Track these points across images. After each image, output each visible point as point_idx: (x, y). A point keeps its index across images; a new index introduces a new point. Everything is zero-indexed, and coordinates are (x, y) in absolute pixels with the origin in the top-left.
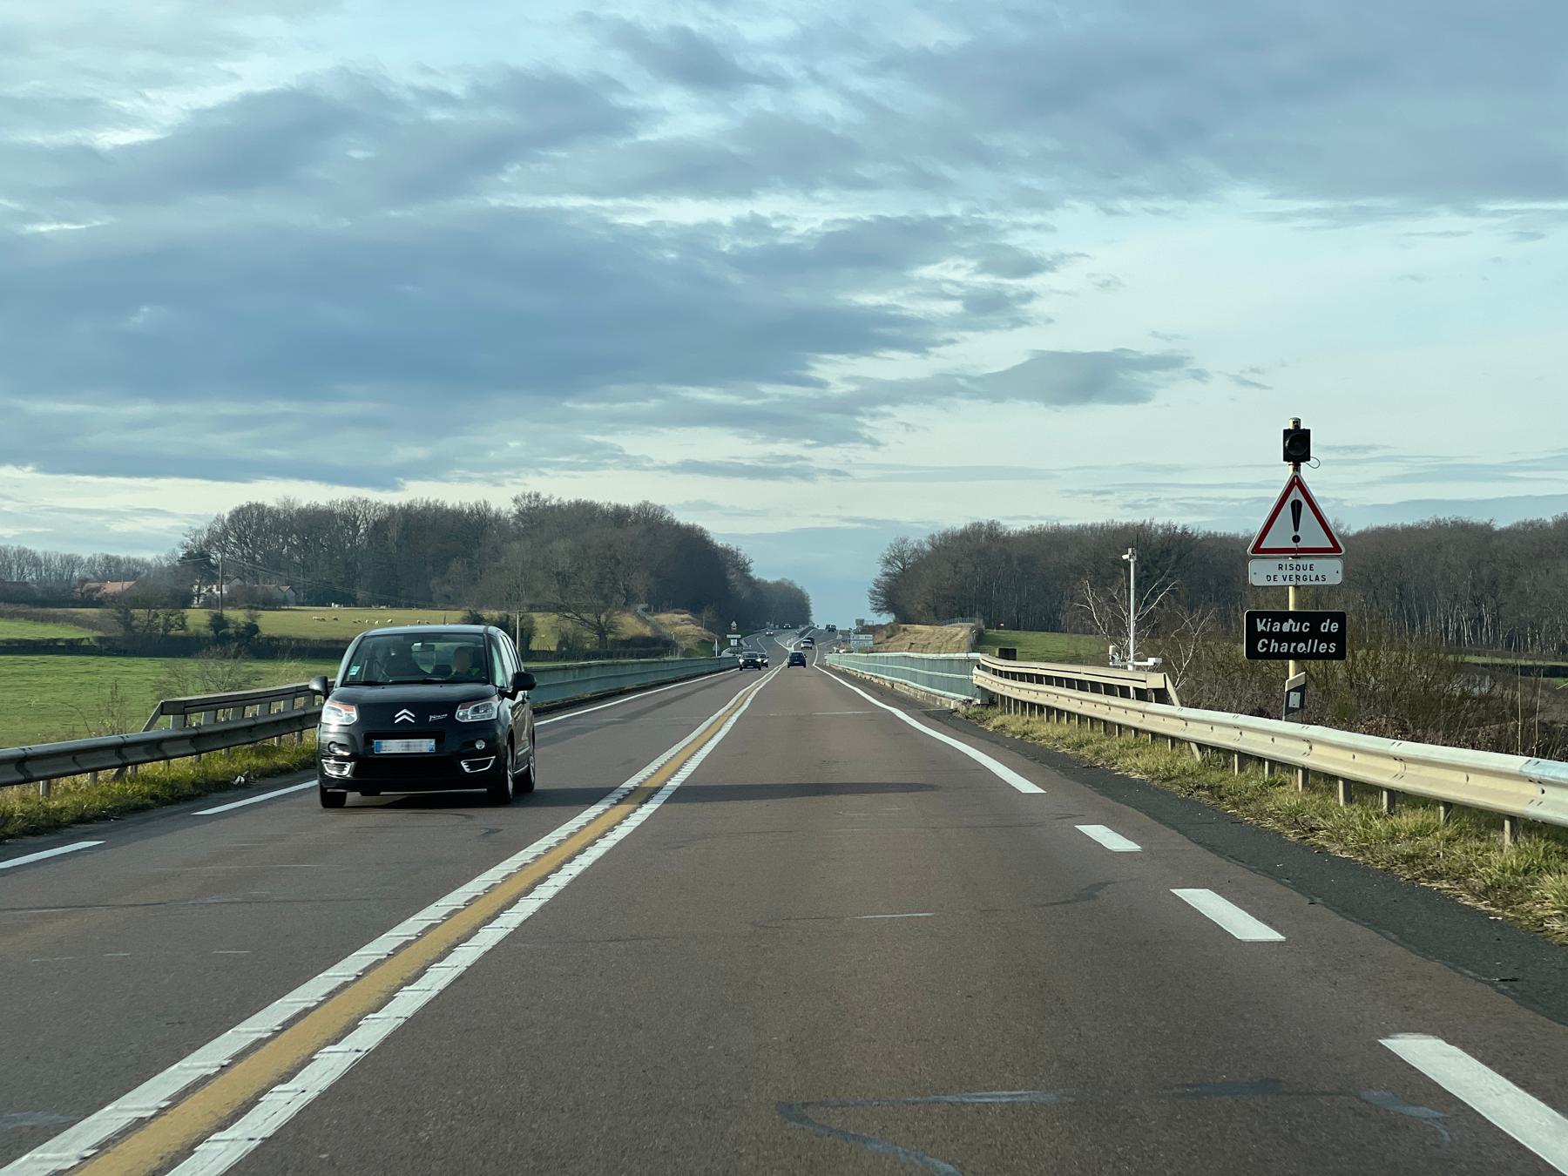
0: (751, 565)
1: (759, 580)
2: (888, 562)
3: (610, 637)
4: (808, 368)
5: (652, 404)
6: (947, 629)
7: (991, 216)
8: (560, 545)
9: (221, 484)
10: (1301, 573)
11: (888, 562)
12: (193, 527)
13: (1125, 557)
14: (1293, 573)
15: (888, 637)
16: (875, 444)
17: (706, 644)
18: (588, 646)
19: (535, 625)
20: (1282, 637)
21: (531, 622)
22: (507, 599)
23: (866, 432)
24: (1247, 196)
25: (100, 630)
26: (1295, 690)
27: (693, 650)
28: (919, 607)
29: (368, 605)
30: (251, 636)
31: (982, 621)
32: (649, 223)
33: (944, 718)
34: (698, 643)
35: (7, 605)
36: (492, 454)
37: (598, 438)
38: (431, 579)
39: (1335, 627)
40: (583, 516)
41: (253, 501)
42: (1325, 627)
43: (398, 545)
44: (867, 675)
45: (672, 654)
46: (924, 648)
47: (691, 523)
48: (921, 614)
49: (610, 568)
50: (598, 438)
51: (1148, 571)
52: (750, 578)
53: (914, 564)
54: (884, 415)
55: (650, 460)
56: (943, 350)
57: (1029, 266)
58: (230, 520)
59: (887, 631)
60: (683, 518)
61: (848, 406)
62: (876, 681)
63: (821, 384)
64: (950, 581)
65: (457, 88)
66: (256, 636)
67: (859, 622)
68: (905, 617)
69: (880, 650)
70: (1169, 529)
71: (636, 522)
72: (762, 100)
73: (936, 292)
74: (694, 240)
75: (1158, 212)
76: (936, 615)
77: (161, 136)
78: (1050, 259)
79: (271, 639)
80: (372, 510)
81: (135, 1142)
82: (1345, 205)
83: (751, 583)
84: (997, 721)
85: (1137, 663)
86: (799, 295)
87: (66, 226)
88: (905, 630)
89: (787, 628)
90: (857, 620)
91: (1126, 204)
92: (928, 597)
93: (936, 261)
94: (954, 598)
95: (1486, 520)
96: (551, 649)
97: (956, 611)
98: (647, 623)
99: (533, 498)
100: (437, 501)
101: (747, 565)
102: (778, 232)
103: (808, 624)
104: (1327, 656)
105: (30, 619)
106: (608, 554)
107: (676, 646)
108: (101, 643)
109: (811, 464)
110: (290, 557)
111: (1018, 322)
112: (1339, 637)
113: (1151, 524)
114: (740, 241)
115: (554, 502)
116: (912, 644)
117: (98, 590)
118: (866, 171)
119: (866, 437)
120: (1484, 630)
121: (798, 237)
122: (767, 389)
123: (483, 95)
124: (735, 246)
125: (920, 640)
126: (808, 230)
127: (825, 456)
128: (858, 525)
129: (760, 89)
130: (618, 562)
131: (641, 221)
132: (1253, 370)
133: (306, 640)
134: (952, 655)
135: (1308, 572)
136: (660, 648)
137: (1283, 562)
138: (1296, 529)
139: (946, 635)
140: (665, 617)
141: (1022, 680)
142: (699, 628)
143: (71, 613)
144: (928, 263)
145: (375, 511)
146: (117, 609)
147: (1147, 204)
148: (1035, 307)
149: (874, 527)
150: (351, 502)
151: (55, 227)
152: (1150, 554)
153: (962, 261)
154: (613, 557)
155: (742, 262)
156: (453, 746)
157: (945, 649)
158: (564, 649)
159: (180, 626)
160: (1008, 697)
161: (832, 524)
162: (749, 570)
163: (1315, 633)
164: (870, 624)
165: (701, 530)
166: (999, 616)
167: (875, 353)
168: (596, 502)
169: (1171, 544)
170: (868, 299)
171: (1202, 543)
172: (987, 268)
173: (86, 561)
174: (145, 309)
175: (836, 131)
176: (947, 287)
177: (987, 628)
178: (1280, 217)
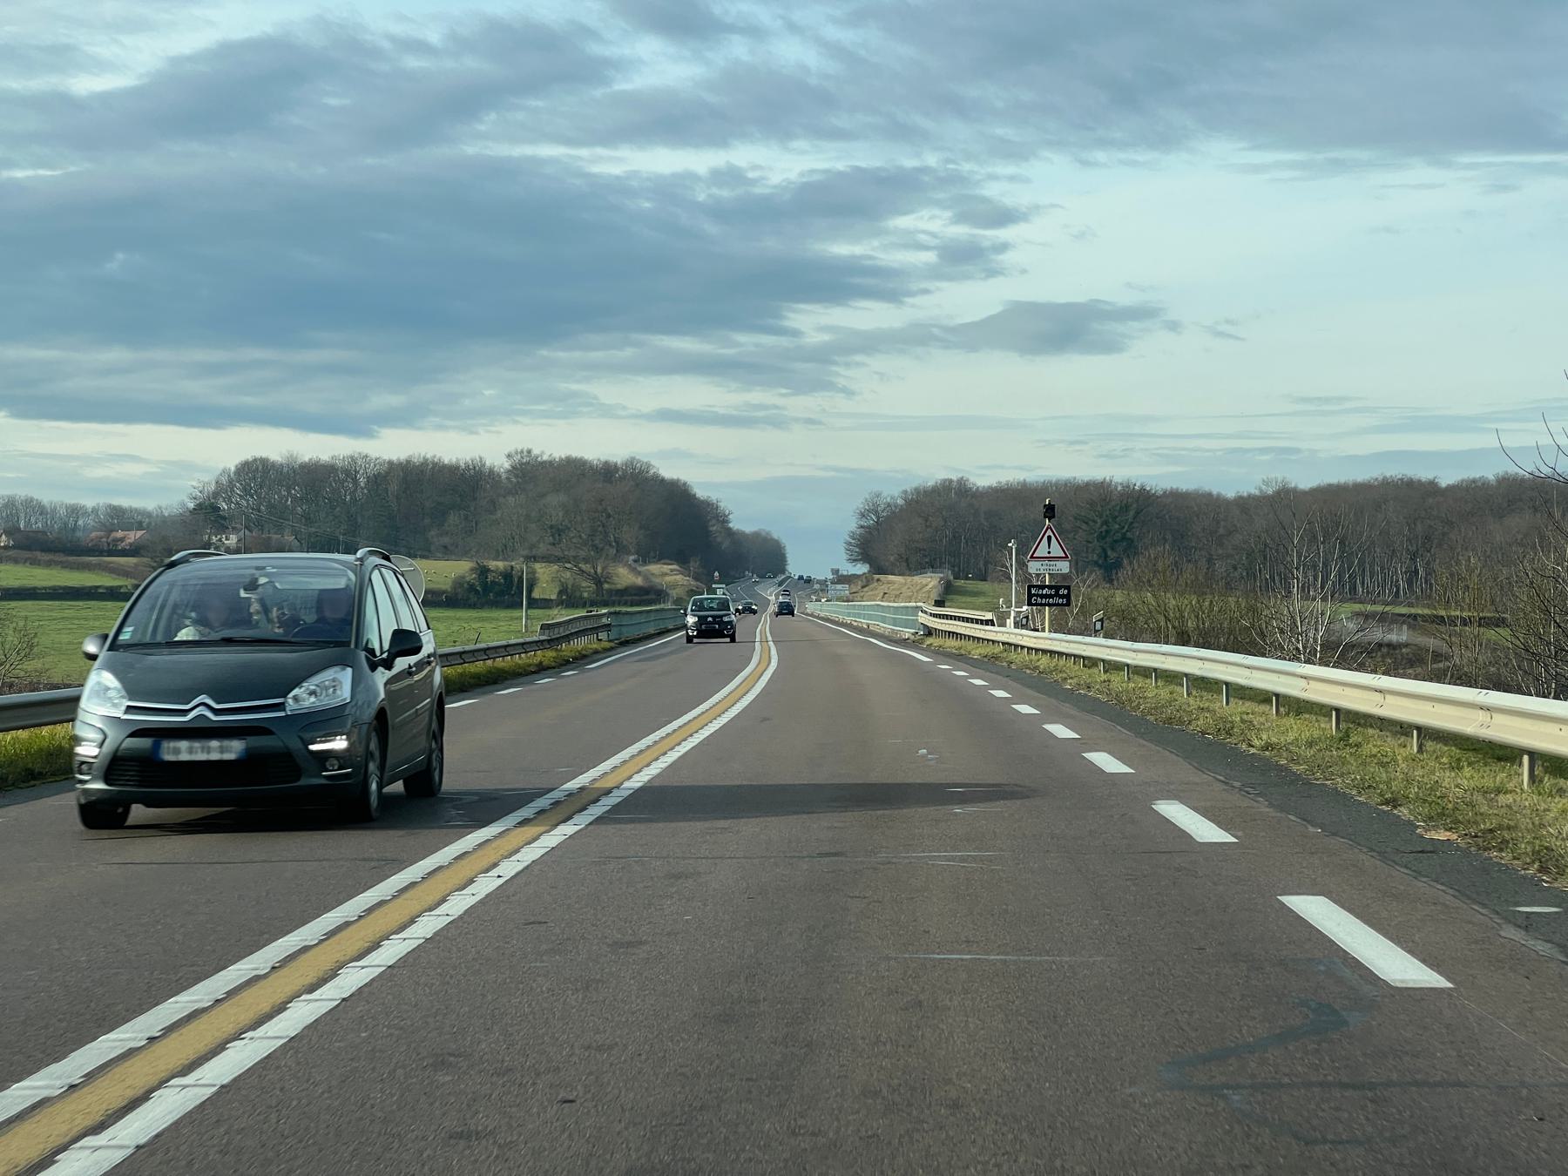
0: (731, 517)
1: (738, 530)
2: (863, 515)
5: (628, 352)
6: (917, 579)
7: (966, 167)
8: (554, 500)
9: (194, 431)
10: (1051, 568)
11: (863, 515)
12: (201, 479)
13: (1010, 545)
14: (1048, 567)
15: (863, 587)
16: (849, 393)
18: (585, 595)
19: (537, 575)
20: (1042, 596)
21: (534, 572)
22: (503, 551)
23: (841, 382)
25: (134, 578)
26: (1098, 621)
31: (950, 572)
32: (626, 172)
33: (904, 642)
35: (43, 554)
36: (467, 402)
37: (575, 387)
38: (430, 531)
39: (1066, 592)
40: (573, 473)
41: (258, 455)
42: (1061, 592)
43: (398, 498)
44: (848, 620)
45: (664, 602)
46: (897, 597)
47: (675, 477)
50: (575, 387)
51: (1108, 526)
52: (730, 529)
53: (887, 518)
54: (858, 364)
55: (624, 408)
56: (917, 300)
57: (1004, 217)
59: (862, 581)
60: (668, 472)
61: (823, 356)
62: (855, 624)
63: (795, 333)
65: (434, 36)
67: (835, 572)
68: (879, 569)
69: (856, 599)
70: (1128, 487)
71: (622, 478)
72: (738, 49)
74: (668, 190)
75: (1134, 164)
77: (137, 82)
78: (1024, 210)
80: (372, 464)
81: (248, 996)
82: (1320, 157)
83: (730, 533)
84: (928, 643)
85: (1017, 610)
86: (772, 244)
87: (42, 172)
88: (878, 580)
89: (770, 577)
90: (832, 570)
91: (1101, 156)
94: (925, 550)
95: (1431, 477)
97: (927, 563)
98: (640, 573)
100: (435, 456)
101: (727, 516)
102: (754, 182)
103: (784, 573)
104: (1062, 605)
105: (66, 567)
106: (600, 508)
107: (668, 595)
109: (786, 413)
110: (294, 509)
111: (992, 273)
112: (1068, 597)
114: (715, 191)
115: (545, 458)
116: (885, 593)
117: (122, 540)
118: (842, 121)
120: (1419, 583)
121: (775, 187)
123: (460, 44)
126: (784, 180)
127: (800, 404)
128: (832, 474)
129: (736, 38)
130: (609, 516)
131: (615, 170)
132: (1228, 322)
134: (907, 604)
135: (1054, 567)
136: (652, 596)
137: (1044, 563)
138: (1049, 548)
139: (917, 585)
140: (655, 568)
141: (977, 623)
143: (105, 562)
144: (905, 213)
145: (375, 466)
146: (152, 558)
147: (1122, 156)
148: (1007, 258)
150: (352, 457)
151: (30, 173)
153: (937, 212)
154: (605, 510)
155: (718, 212)
156: (723, 627)
157: (916, 598)
158: (564, 597)
160: (936, 629)
162: (728, 522)
163: (1057, 594)
164: (845, 573)
165: (685, 484)
166: (967, 567)
167: (850, 303)
168: (586, 458)
169: (1130, 500)
171: (1159, 500)
173: (90, 510)
174: (120, 256)
175: (813, 81)
176: (922, 238)
177: (954, 578)
178: (1256, 169)
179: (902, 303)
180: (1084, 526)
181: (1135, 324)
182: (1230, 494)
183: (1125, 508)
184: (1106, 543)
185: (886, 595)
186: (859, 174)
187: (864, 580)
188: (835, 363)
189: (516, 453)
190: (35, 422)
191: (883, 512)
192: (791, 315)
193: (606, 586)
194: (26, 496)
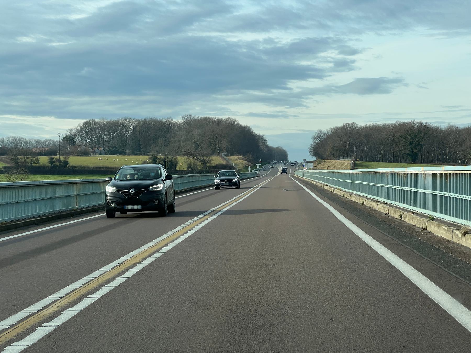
3: (208, 165)
4: (288, 84)
5: (239, 96)
11: (315, 138)
17: (246, 167)
23: (305, 104)
24: (421, 29)
27: (241, 170)
28: (328, 154)
29: (129, 154)
30: (65, 166)
34: (244, 167)
37: (223, 106)
40: (207, 122)
46: (333, 168)
47: (245, 125)
48: (328, 156)
49: (213, 140)
50: (223, 106)
51: (413, 139)
52: (267, 145)
54: (310, 98)
55: (239, 113)
56: (328, 78)
57: (354, 52)
58: (83, 125)
63: (291, 89)
64: (339, 144)
66: (67, 166)
67: (305, 160)
73: (326, 61)
74: (251, 46)
76: (334, 156)
78: (360, 50)
79: (73, 167)
83: (267, 147)
86: (283, 62)
88: (324, 161)
91: (384, 32)
92: (331, 150)
93: (325, 51)
96: (185, 170)
98: (225, 159)
99: (189, 116)
102: (277, 43)
108: (5, 169)
109: (287, 113)
111: (351, 69)
113: (414, 122)
114: (265, 46)
115: (196, 117)
116: (328, 166)
119: (304, 105)
121: (284, 44)
122: (275, 91)
124: (264, 47)
125: (331, 165)
127: (292, 111)
130: (217, 138)
131: (235, 40)
132: (423, 83)
133: (88, 167)
140: (232, 157)
142: (245, 161)
148: (354, 65)
149: (307, 132)
151: (58, 44)
152: (414, 133)
153: (333, 51)
155: (266, 52)
157: (342, 168)
159: (37, 162)
161: (294, 132)
162: (267, 143)
165: (249, 127)
170: (304, 63)
172: (341, 53)
174: (86, 69)
175: (295, 11)
178: (431, 35)
179: (323, 79)
180: (404, 140)
181: (394, 84)
182: (462, 127)
183: (420, 132)
184: (412, 146)
185: (329, 167)
186: (311, 40)
187: (318, 161)
188: (303, 98)
189: (185, 116)
190: (62, 120)
191: (322, 137)
192: (288, 83)
193: (208, 165)
194: (19, 137)
